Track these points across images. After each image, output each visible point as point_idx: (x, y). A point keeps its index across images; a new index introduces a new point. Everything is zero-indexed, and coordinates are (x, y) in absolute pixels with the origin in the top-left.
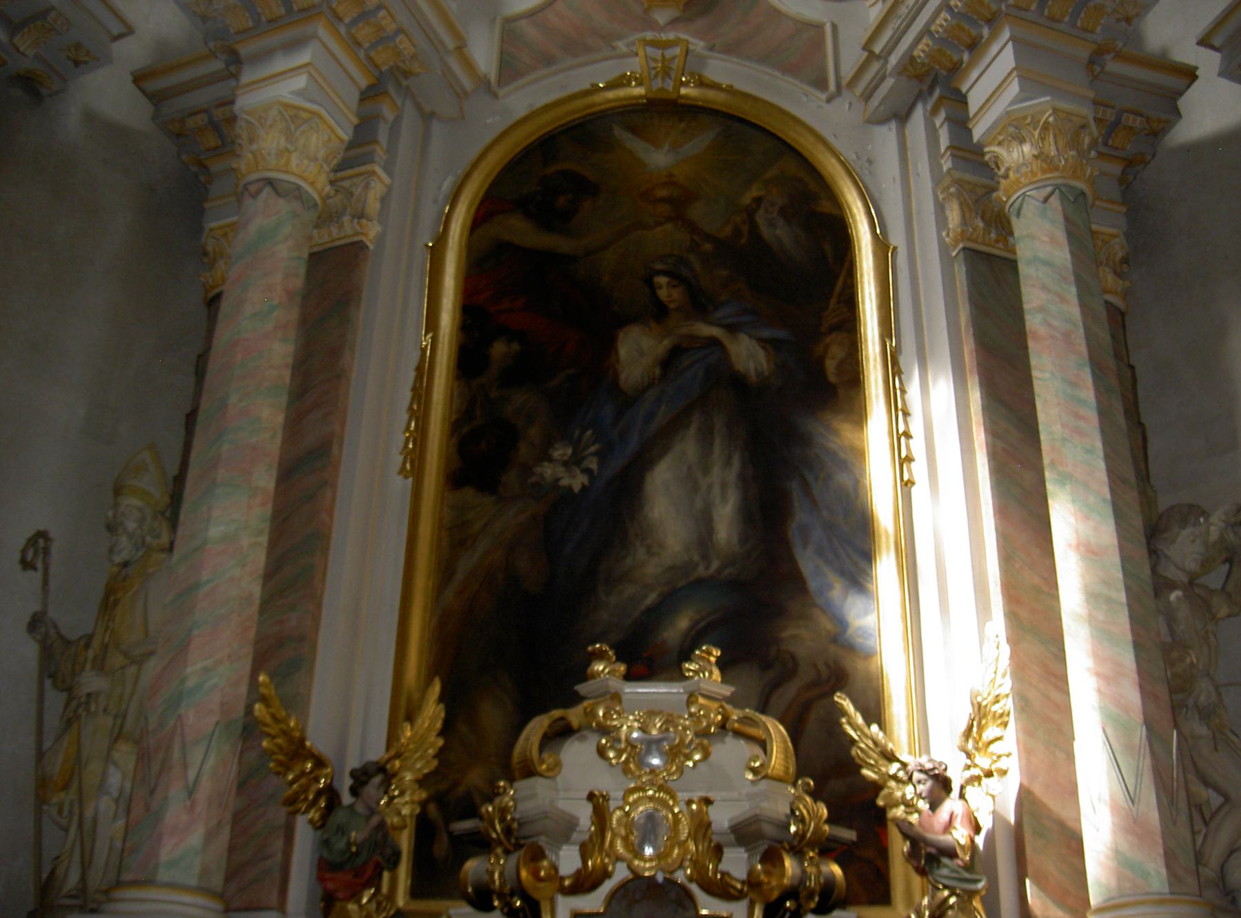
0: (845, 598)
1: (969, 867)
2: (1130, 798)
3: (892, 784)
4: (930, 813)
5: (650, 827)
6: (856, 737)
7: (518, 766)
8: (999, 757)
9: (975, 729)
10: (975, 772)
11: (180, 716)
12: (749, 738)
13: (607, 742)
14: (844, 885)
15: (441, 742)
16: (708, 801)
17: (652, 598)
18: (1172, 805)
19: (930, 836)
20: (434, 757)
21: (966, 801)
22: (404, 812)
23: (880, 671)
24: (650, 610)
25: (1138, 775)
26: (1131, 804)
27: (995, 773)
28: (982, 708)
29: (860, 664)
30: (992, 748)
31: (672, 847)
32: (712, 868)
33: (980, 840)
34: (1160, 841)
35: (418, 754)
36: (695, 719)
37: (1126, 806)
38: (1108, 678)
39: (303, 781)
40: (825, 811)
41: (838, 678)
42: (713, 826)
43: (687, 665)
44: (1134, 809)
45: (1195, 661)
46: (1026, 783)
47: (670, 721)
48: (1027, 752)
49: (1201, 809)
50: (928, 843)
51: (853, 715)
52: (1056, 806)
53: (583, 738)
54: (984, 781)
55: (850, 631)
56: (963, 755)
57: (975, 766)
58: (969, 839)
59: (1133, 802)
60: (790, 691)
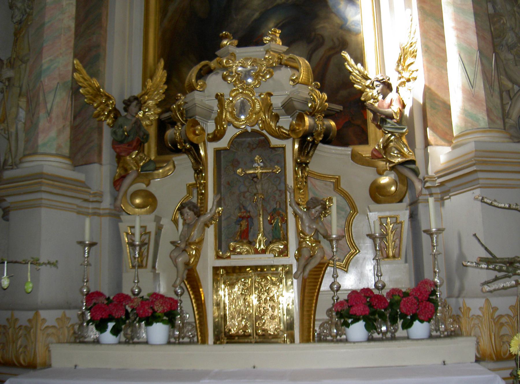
0: (346, 8)
1: (400, 122)
2: (471, 85)
3: (368, 90)
4: (382, 100)
5: (242, 108)
6: (351, 71)
7: (188, 87)
8: (413, 72)
9: (402, 60)
10: (403, 80)
11: (41, 82)
12: (292, 67)
13: (226, 73)
14: (335, 127)
15: (166, 87)
16: (270, 95)
17: (257, 15)
18: (491, 88)
19: (381, 110)
20: (163, 93)
21: (399, 94)
22: (151, 118)
23: (362, 40)
24: (256, 20)
25: (475, 74)
26: (471, 88)
27: (411, 80)
28: (405, 50)
29: (353, 38)
30: (410, 68)
31: (252, 115)
33: (407, 112)
34: (485, 104)
35: (156, 93)
36: (267, 60)
37: (469, 89)
38: (461, 30)
39: (102, 106)
40: (326, 97)
41: (344, 45)
42: (274, 106)
43: (265, 38)
44: (473, 90)
45: (505, 22)
46: (427, 84)
47: (254, 61)
48: (428, 71)
49: (509, 93)
50: (382, 113)
51: (350, 61)
52: (441, 94)
53: (217, 73)
54: (407, 83)
55: (348, 23)
56: (397, 73)
57: (403, 77)
58: (399, 109)
59: (472, 87)
60: (321, 52)
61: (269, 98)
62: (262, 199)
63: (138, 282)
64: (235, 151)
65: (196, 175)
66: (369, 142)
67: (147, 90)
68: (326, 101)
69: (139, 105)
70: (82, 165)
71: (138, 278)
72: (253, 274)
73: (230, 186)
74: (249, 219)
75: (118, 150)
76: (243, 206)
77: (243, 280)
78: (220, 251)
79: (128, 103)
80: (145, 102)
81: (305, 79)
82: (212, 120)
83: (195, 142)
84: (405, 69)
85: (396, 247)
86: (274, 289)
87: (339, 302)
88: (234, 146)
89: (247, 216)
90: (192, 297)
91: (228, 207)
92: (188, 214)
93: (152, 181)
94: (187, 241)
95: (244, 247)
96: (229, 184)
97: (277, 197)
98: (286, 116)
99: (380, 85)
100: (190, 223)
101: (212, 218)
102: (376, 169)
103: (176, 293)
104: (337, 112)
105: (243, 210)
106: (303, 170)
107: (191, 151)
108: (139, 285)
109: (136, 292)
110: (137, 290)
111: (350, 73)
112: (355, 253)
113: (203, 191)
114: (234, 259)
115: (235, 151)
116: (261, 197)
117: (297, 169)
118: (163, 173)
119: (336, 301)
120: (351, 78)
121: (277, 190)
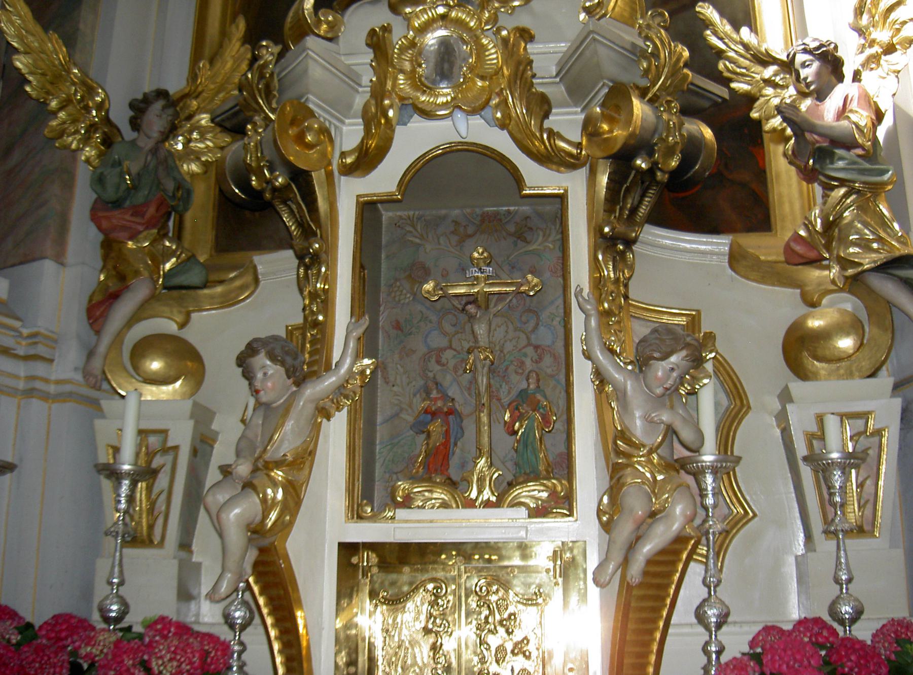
3: (769, 91)
6: (723, 47)
10: (876, 49)
27: (897, 47)
30: (893, 16)
32: (591, 322)
33: (881, 133)
56: (856, 34)
61: (523, 45)
62: (488, 362)
63: (121, 583)
64: (417, 241)
65: (302, 271)
66: (773, 226)
67: (197, 87)
68: (686, 65)
69: (170, 111)
70: (13, 265)
71: (121, 572)
72: (462, 567)
73: (402, 331)
74: (451, 417)
75: (105, 224)
76: (437, 384)
77: (430, 586)
78: (366, 505)
79: (142, 105)
80: (190, 117)
81: (622, 6)
82: (355, 117)
83: (302, 165)
84: (877, 22)
85: (867, 502)
86: (528, 617)
87: (727, 664)
88: (416, 230)
89: (445, 410)
90: (273, 633)
91: (395, 389)
92: (265, 374)
93: (194, 316)
94: (257, 459)
95: (435, 495)
96: (398, 326)
97: (528, 362)
98: (568, 106)
99: (811, 61)
100: (275, 402)
101: (341, 390)
102: (799, 291)
103: (228, 620)
104: (715, 104)
105: (434, 394)
106: (619, 260)
107: (290, 200)
108: (123, 591)
109: (111, 611)
110: (115, 607)
111: (720, 54)
112: (744, 521)
113: (321, 318)
114: (407, 521)
115: (417, 241)
116: (486, 358)
117: (600, 257)
118: (223, 295)
119: (714, 656)
120: (721, 66)
121: (529, 344)
